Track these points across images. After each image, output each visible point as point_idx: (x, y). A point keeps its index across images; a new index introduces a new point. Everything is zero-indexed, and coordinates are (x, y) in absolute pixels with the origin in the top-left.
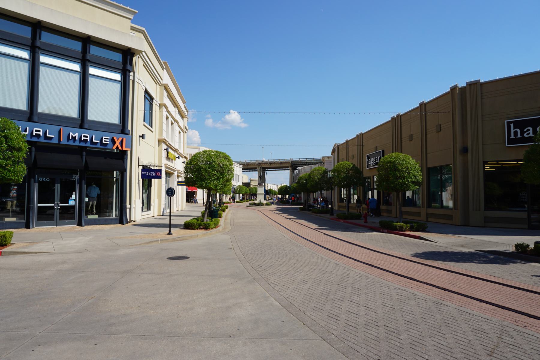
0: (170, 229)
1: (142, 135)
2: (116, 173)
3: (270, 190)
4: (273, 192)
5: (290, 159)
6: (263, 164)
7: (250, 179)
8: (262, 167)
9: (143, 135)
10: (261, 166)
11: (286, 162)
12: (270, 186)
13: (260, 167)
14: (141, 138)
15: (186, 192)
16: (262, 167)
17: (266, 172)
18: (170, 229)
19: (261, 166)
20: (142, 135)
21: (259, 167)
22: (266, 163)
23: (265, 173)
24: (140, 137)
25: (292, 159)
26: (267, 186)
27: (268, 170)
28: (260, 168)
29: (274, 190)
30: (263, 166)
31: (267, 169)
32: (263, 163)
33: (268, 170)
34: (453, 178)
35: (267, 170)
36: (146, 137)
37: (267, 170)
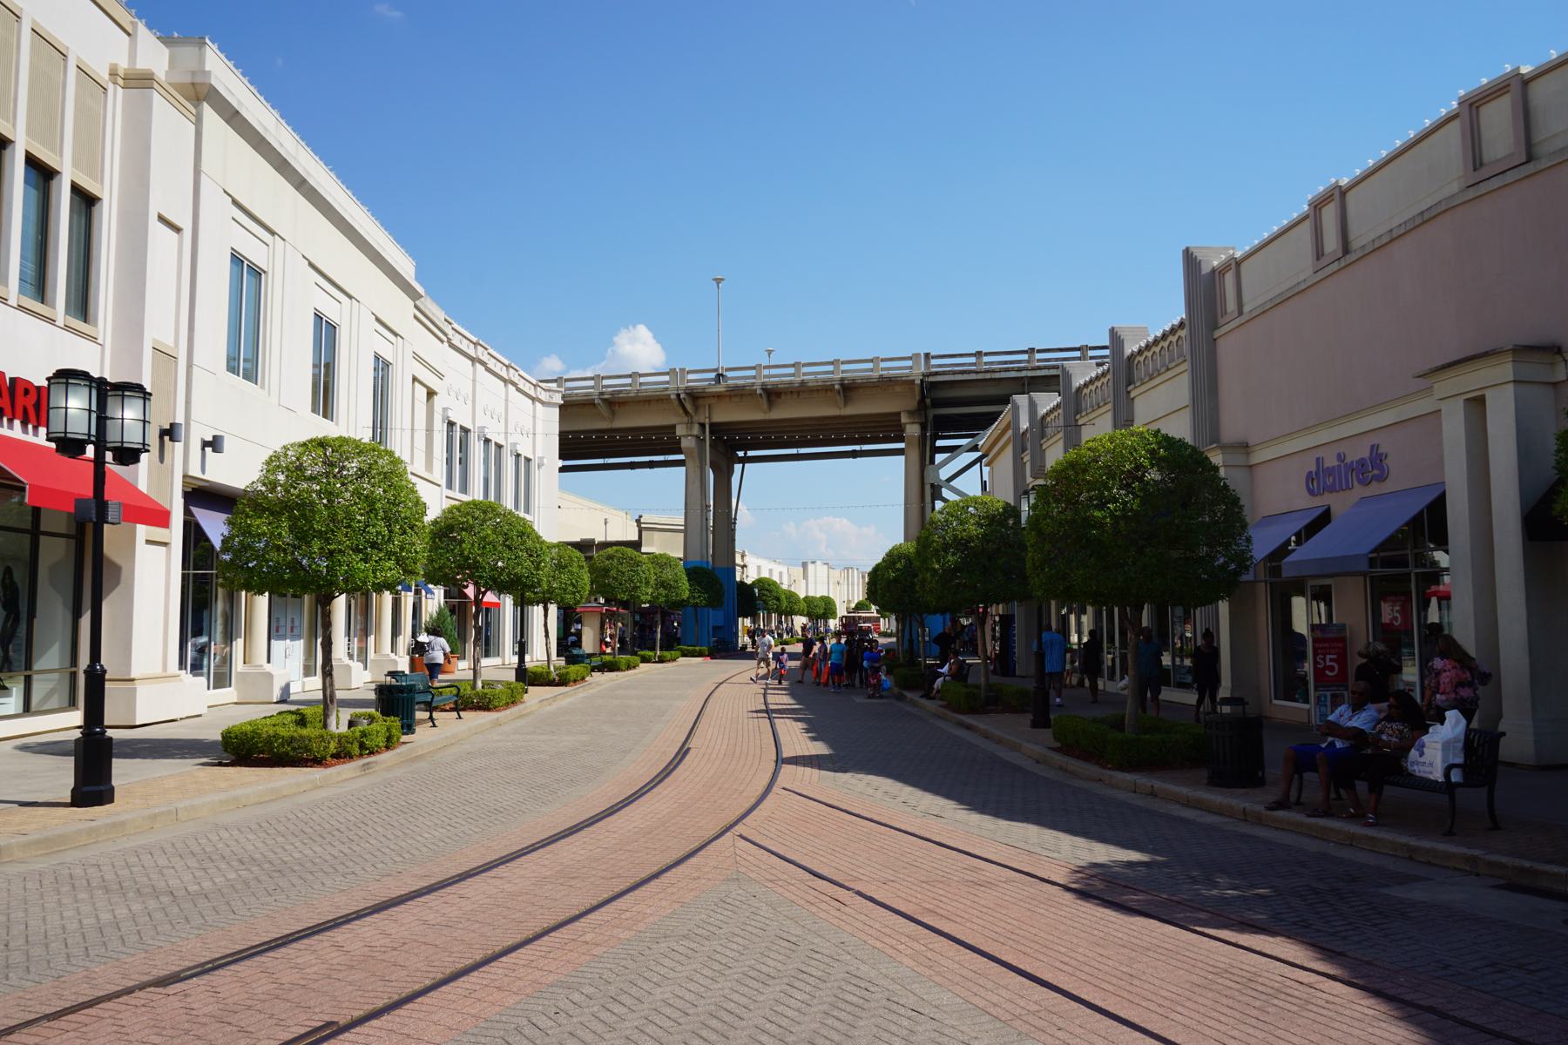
0: (522, 660)
1: (211, 439)
2: (764, 614)
3: (765, 585)
4: (778, 599)
5: (916, 356)
6: (719, 396)
7: (638, 521)
8: (712, 425)
9: (214, 437)
10: (703, 417)
11: (886, 384)
12: (759, 567)
13: (702, 426)
14: (208, 450)
15: (1447, 544)
16: (712, 425)
17: (738, 467)
18: (522, 660)
19: (703, 417)
20: (168, 427)
21: (690, 424)
22: (739, 394)
23: (731, 472)
24: (205, 444)
25: (927, 356)
26: (744, 566)
27: (750, 453)
28: (696, 430)
29: (785, 587)
30: (724, 415)
31: (746, 450)
32: (720, 388)
33: (750, 453)
34: (589, 605)
35: (741, 454)
36: (227, 445)
37: (741, 454)
